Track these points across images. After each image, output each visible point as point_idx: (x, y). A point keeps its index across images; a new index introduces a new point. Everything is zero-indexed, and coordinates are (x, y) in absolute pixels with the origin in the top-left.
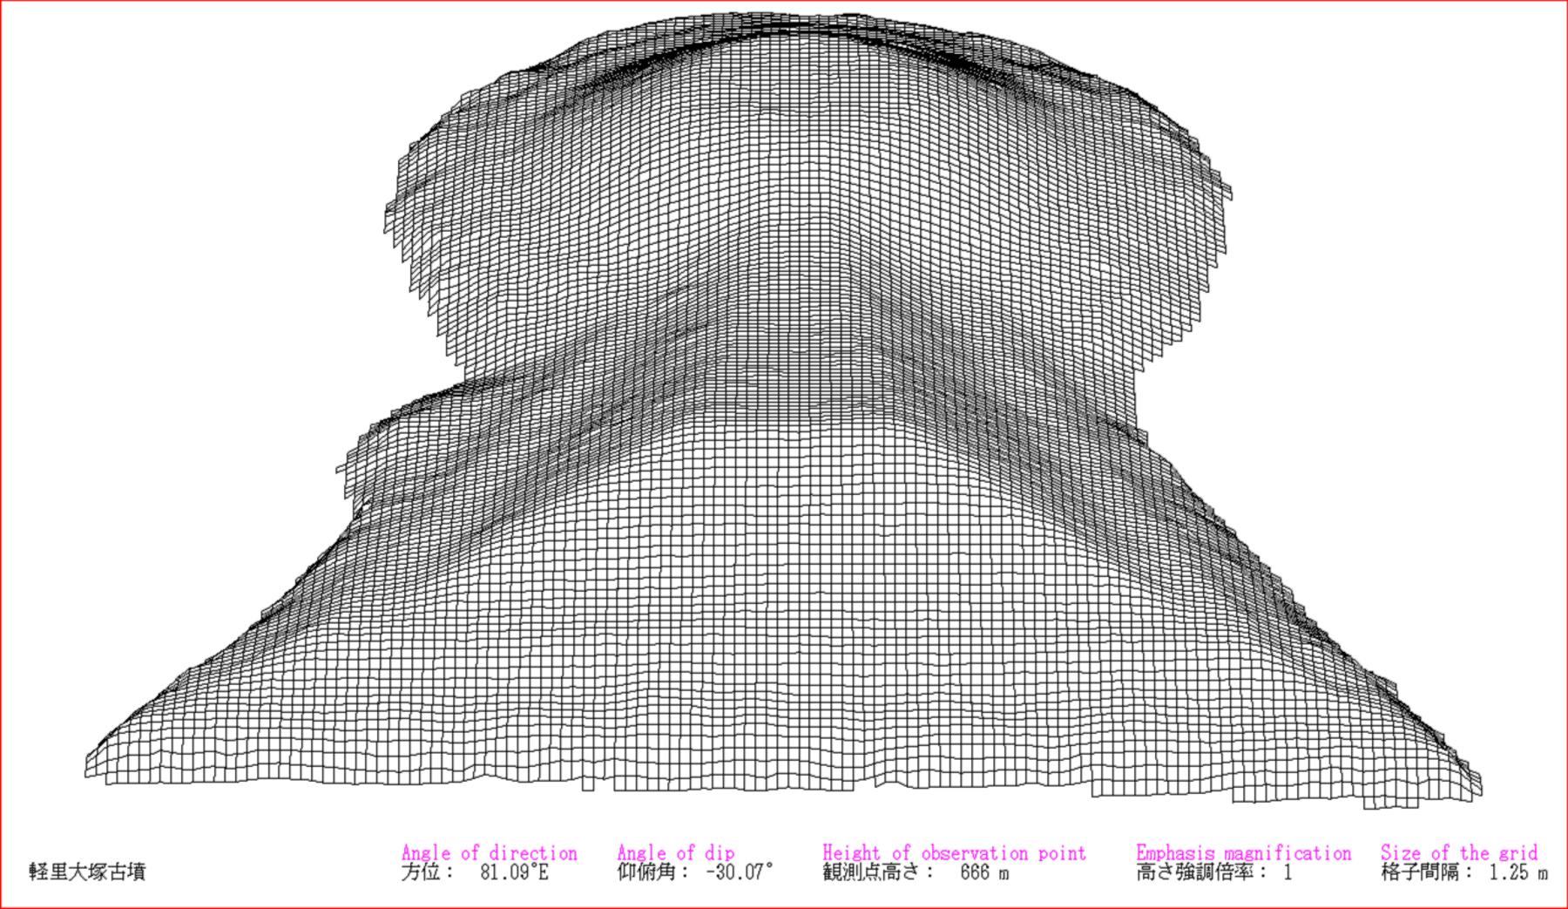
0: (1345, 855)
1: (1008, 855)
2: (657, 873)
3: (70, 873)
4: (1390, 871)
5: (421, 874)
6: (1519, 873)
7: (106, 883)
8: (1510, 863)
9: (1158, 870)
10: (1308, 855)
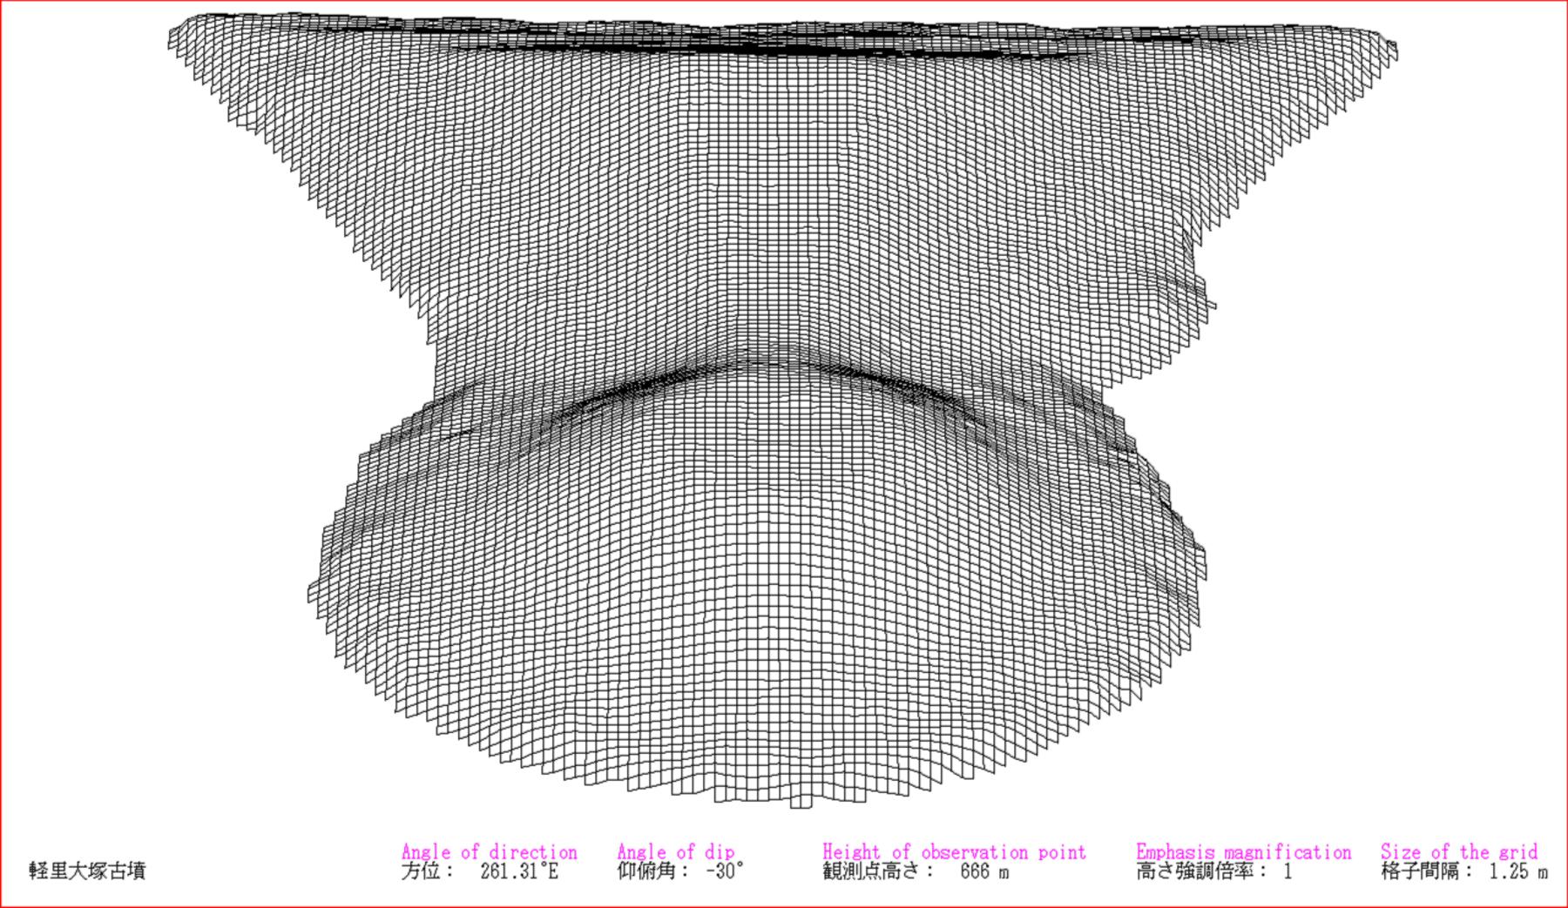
0: (1345, 854)
1: (1008, 854)
2: (657, 873)
3: (70, 872)
4: (1390, 870)
5: (421, 873)
6: (1519, 872)
7: (106, 882)
8: (1510, 862)
9: (1158, 870)
10: (1308, 854)
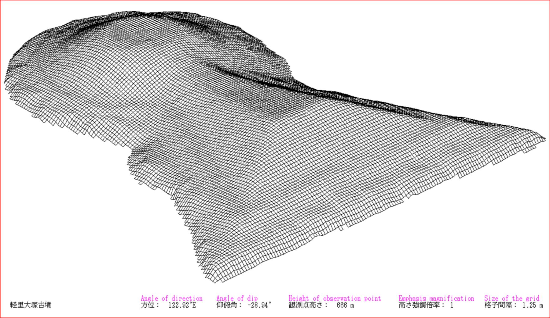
0: (472, 299)
1: (353, 299)
2: (231, 306)
3: (24, 305)
4: (488, 305)
5: (148, 306)
6: (533, 305)
7: (37, 309)
8: (530, 302)
9: (406, 305)
10: (459, 299)
